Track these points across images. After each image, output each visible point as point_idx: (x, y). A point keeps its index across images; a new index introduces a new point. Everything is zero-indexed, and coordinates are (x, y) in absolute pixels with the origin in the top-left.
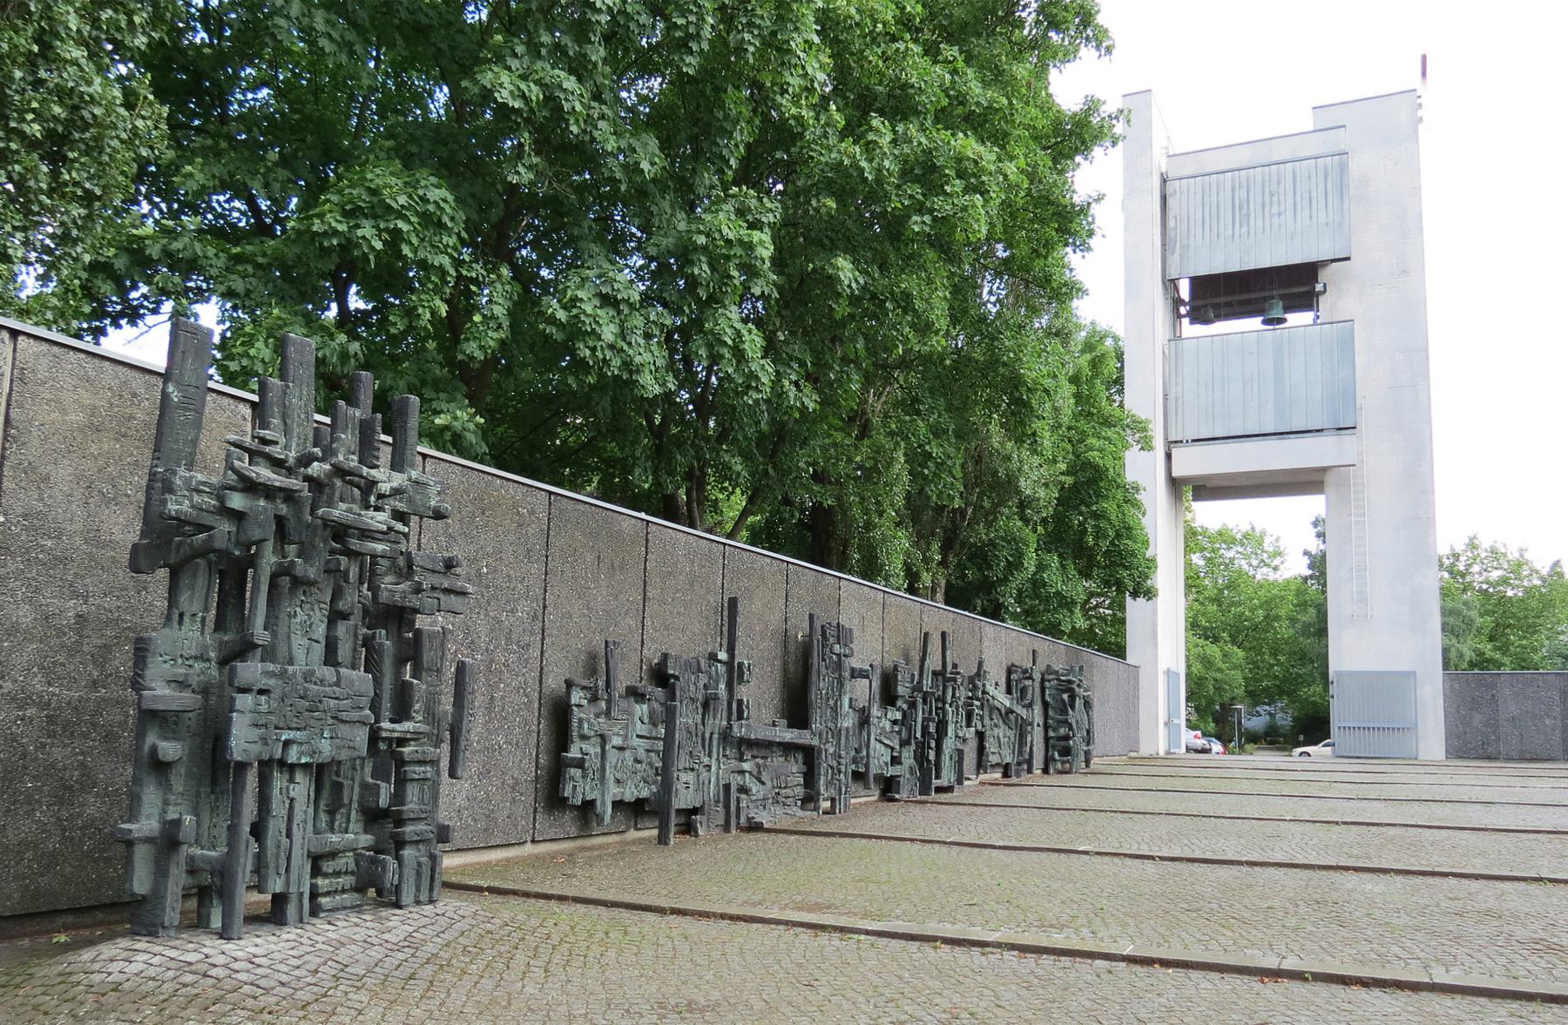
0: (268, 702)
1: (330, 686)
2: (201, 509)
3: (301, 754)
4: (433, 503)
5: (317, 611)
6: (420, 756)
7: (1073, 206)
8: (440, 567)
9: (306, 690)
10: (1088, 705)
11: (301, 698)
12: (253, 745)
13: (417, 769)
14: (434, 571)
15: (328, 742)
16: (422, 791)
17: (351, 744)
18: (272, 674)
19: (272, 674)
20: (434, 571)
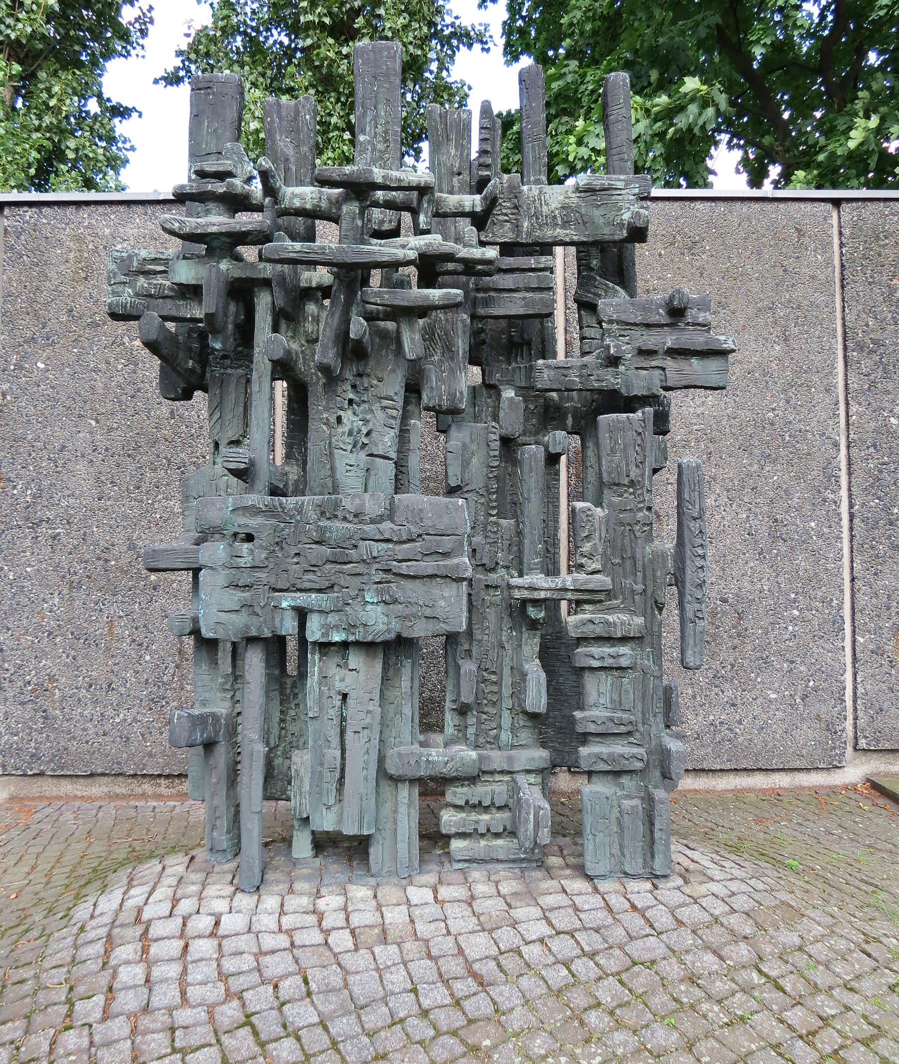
0: (251, 552)
1: (372, 521)
2: (150, 296)
3: (328, 628)
4: (626, 216)
5: (380, 415)
6: (599, 631)
7: (172, 73)
8: (661, 316)
9: (322, 530)
10: (283, 396)
11: (317, 543)
12: (233, 616)
13: (595, 650)
14: (648, 326)
15: (380, 608)
16: (618, 688)
17: (428, 612)
18: (254, 511)
19: (254, 511)
20: (648, 326)
